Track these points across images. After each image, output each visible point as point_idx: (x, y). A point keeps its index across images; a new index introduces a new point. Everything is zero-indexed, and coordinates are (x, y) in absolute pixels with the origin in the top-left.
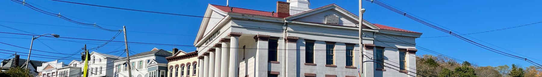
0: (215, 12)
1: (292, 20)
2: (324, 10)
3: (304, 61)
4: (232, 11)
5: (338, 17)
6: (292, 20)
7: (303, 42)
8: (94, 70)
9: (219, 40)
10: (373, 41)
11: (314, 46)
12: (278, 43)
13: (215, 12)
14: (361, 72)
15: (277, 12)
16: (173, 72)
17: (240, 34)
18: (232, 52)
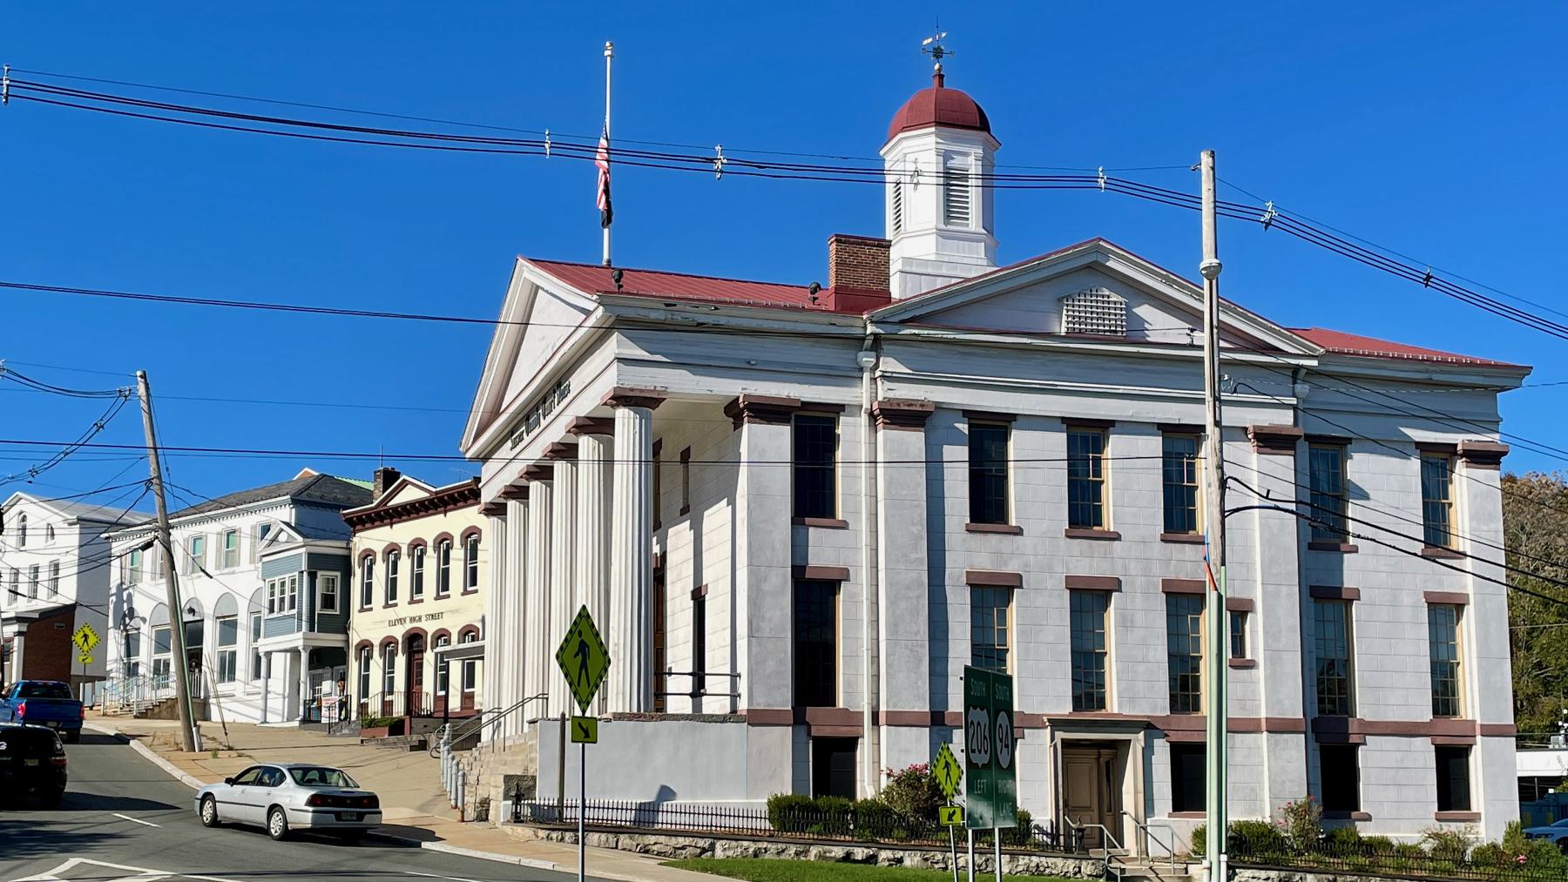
0: (547, 291)
1: (903, 322)
2: (1052, 271)
4: (620, 286)
5: (1120, 299)
6: (903, 322)
7: (956, 425)
8: (21, 578)
9: (565, 423)
10: (1291, 412)
11: (1011, 444)
12: (839, 431)
13: (547, 291)
14: (1218, 563)
15: (832, 284)
16: (374, 581)
17: (659, 392)
18: (626, 480)
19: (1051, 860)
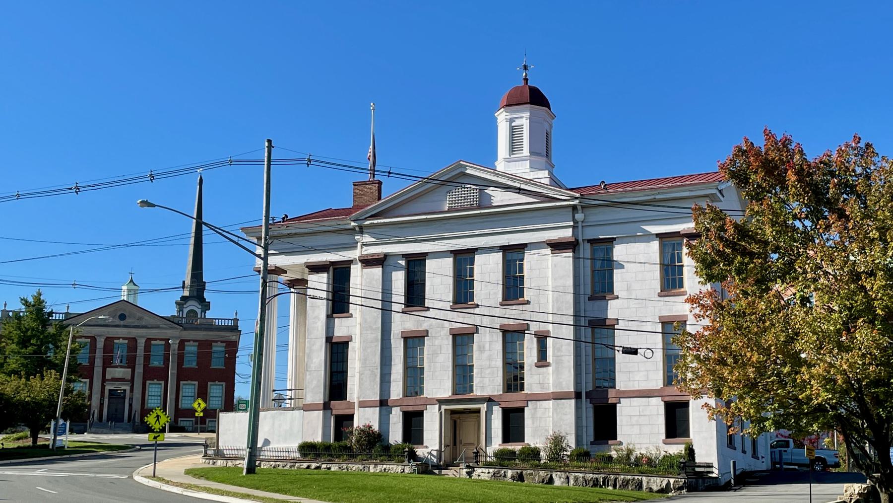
3: (496, 294)
7: (399, 262)
19: (391, 467)
